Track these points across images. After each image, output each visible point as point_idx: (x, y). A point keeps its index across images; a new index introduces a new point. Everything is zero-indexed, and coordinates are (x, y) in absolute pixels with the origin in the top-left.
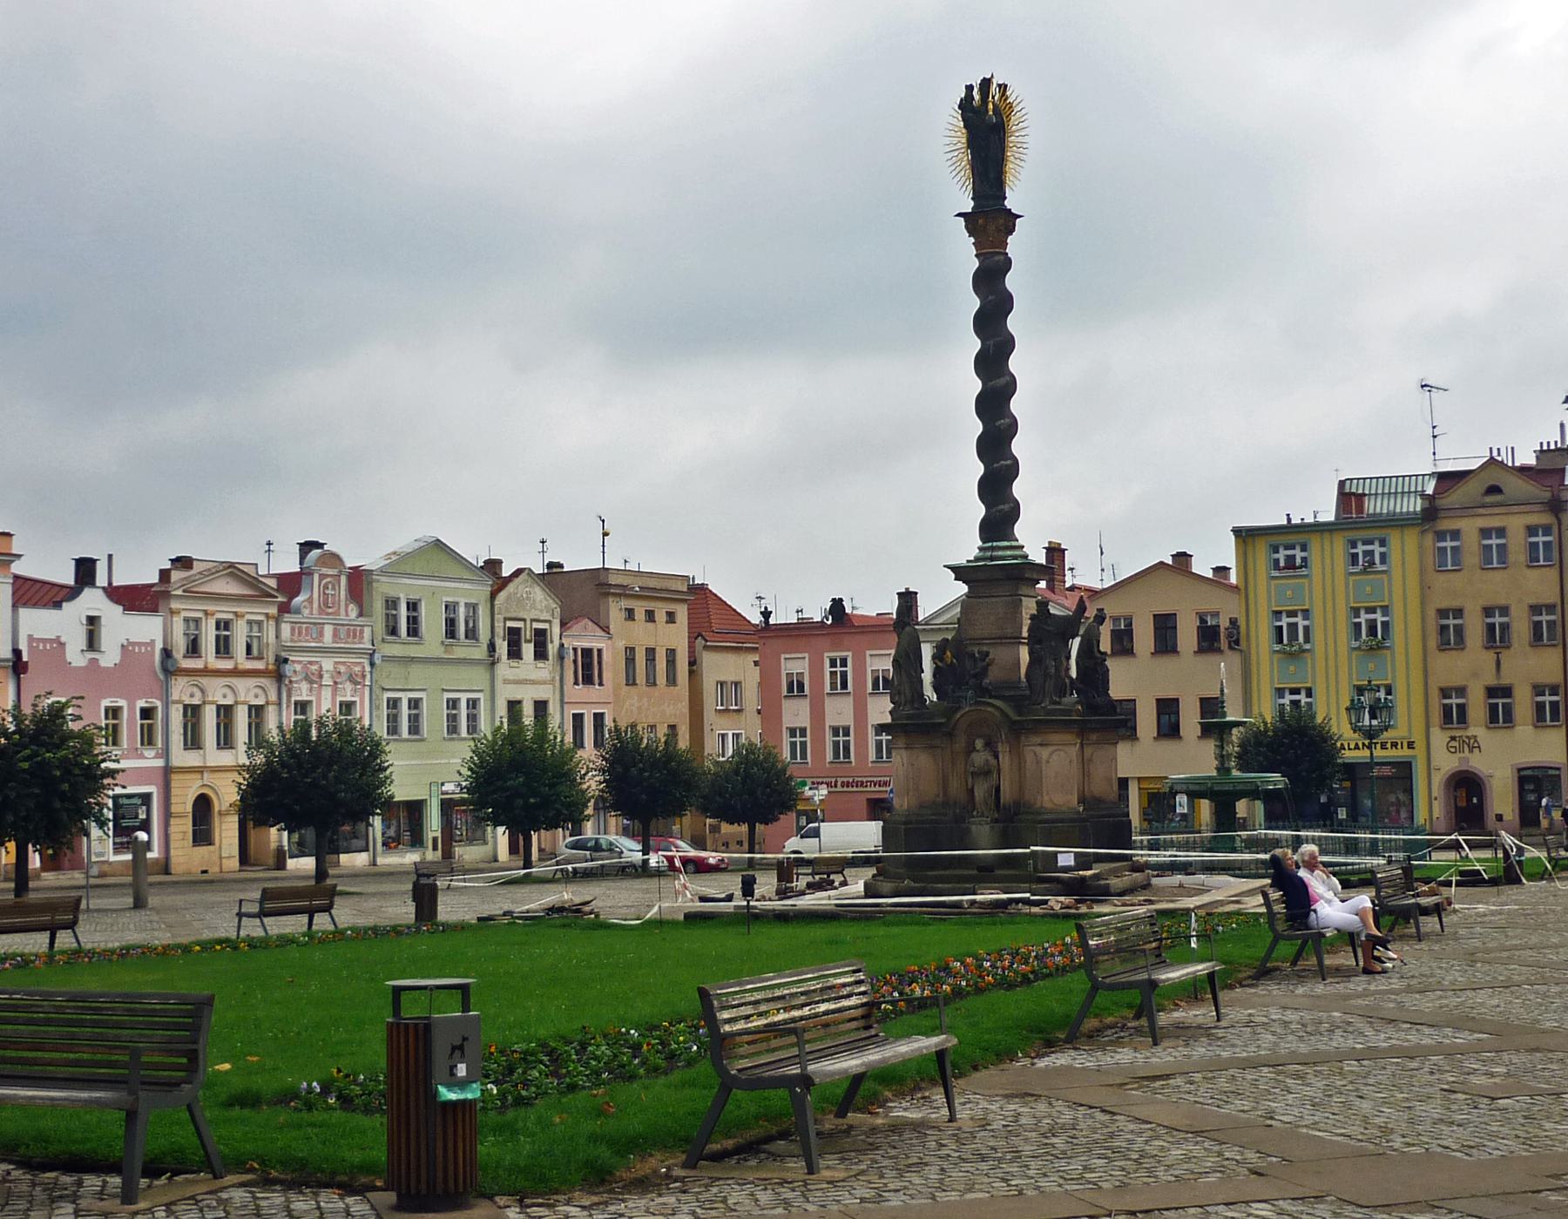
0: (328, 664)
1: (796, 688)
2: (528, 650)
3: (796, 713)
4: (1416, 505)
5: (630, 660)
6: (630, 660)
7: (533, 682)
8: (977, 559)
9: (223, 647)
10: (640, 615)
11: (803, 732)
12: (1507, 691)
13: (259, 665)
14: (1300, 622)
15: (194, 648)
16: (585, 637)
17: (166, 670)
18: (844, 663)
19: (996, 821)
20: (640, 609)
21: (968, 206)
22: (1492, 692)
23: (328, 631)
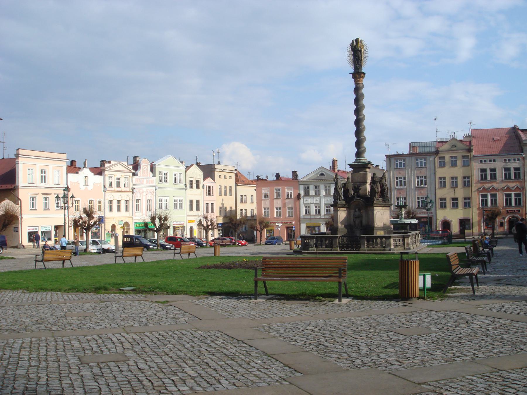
0: (145, 189)
1: (266, 197)
2: (195, 186)
3: (266, 204)
4: (433, 150)
5: (220, 189)
6: (220, 189)
7: (196, 195)
8: (355, 162)
9: (118, 184)
10: (223, 177)
11: (268, 208)
12: (457, 199)
13: (128, 190)
14: (403, 180)
15: (111, 185)
16: (209, 182)
17: (104, 191)
18: (279, 190)
19: (361, 230)
20: (223, 174)
21: (353, 71)
22: (453, 199)
23: (145, 180)
